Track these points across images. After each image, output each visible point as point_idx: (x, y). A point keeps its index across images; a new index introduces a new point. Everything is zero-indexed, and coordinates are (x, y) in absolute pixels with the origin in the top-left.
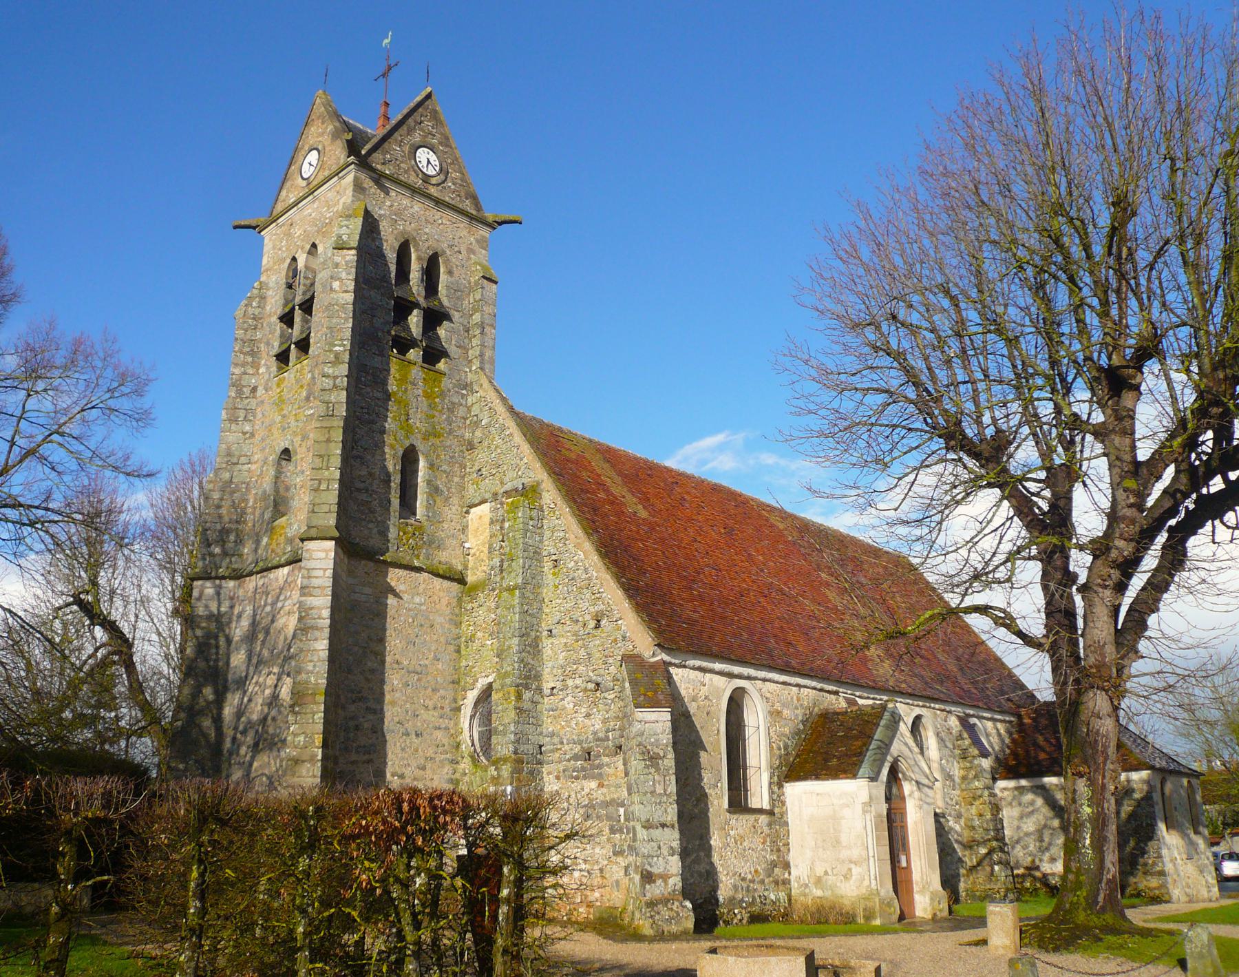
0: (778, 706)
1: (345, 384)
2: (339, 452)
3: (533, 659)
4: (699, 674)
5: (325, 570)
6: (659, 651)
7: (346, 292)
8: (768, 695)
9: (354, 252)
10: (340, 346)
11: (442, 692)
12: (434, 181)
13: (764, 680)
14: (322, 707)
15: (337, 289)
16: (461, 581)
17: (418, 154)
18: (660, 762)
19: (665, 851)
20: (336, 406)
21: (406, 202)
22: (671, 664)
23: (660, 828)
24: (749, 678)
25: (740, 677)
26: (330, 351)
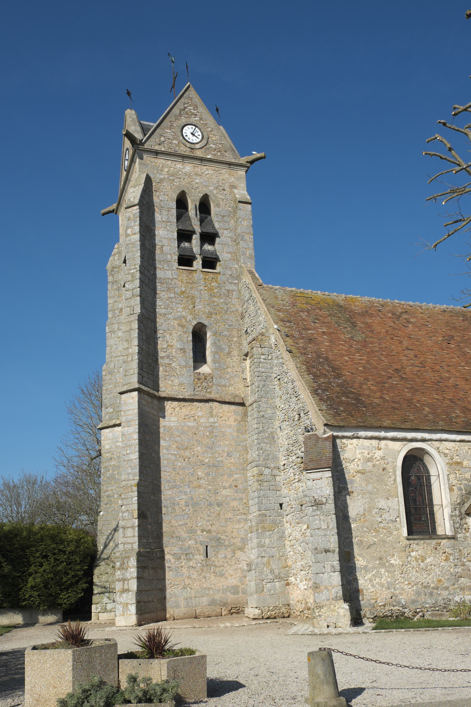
0: (456, 459)
1: (139, 292)
2: (137, 335)
3: (270, 447)
4: (375, 442)
5: (134, 409)
6: (327, 430)
7: (135, 234)
8: (447, 451)
9: (137, 207)
10: (133, 269)
11: (236, 476)
12: (198, 146)
13: (441, 440)
14: (136, 494)
15: (130, 233)
16: (242, 404)
17: (184, 131)
18: (323, 506)
19: (328, 568)
20: (134, 307)
21: (179, 166)
22: (337, 437)
23: (324, 553)
24: (423, 440)
25: (412, 440)
26: (129, 274)
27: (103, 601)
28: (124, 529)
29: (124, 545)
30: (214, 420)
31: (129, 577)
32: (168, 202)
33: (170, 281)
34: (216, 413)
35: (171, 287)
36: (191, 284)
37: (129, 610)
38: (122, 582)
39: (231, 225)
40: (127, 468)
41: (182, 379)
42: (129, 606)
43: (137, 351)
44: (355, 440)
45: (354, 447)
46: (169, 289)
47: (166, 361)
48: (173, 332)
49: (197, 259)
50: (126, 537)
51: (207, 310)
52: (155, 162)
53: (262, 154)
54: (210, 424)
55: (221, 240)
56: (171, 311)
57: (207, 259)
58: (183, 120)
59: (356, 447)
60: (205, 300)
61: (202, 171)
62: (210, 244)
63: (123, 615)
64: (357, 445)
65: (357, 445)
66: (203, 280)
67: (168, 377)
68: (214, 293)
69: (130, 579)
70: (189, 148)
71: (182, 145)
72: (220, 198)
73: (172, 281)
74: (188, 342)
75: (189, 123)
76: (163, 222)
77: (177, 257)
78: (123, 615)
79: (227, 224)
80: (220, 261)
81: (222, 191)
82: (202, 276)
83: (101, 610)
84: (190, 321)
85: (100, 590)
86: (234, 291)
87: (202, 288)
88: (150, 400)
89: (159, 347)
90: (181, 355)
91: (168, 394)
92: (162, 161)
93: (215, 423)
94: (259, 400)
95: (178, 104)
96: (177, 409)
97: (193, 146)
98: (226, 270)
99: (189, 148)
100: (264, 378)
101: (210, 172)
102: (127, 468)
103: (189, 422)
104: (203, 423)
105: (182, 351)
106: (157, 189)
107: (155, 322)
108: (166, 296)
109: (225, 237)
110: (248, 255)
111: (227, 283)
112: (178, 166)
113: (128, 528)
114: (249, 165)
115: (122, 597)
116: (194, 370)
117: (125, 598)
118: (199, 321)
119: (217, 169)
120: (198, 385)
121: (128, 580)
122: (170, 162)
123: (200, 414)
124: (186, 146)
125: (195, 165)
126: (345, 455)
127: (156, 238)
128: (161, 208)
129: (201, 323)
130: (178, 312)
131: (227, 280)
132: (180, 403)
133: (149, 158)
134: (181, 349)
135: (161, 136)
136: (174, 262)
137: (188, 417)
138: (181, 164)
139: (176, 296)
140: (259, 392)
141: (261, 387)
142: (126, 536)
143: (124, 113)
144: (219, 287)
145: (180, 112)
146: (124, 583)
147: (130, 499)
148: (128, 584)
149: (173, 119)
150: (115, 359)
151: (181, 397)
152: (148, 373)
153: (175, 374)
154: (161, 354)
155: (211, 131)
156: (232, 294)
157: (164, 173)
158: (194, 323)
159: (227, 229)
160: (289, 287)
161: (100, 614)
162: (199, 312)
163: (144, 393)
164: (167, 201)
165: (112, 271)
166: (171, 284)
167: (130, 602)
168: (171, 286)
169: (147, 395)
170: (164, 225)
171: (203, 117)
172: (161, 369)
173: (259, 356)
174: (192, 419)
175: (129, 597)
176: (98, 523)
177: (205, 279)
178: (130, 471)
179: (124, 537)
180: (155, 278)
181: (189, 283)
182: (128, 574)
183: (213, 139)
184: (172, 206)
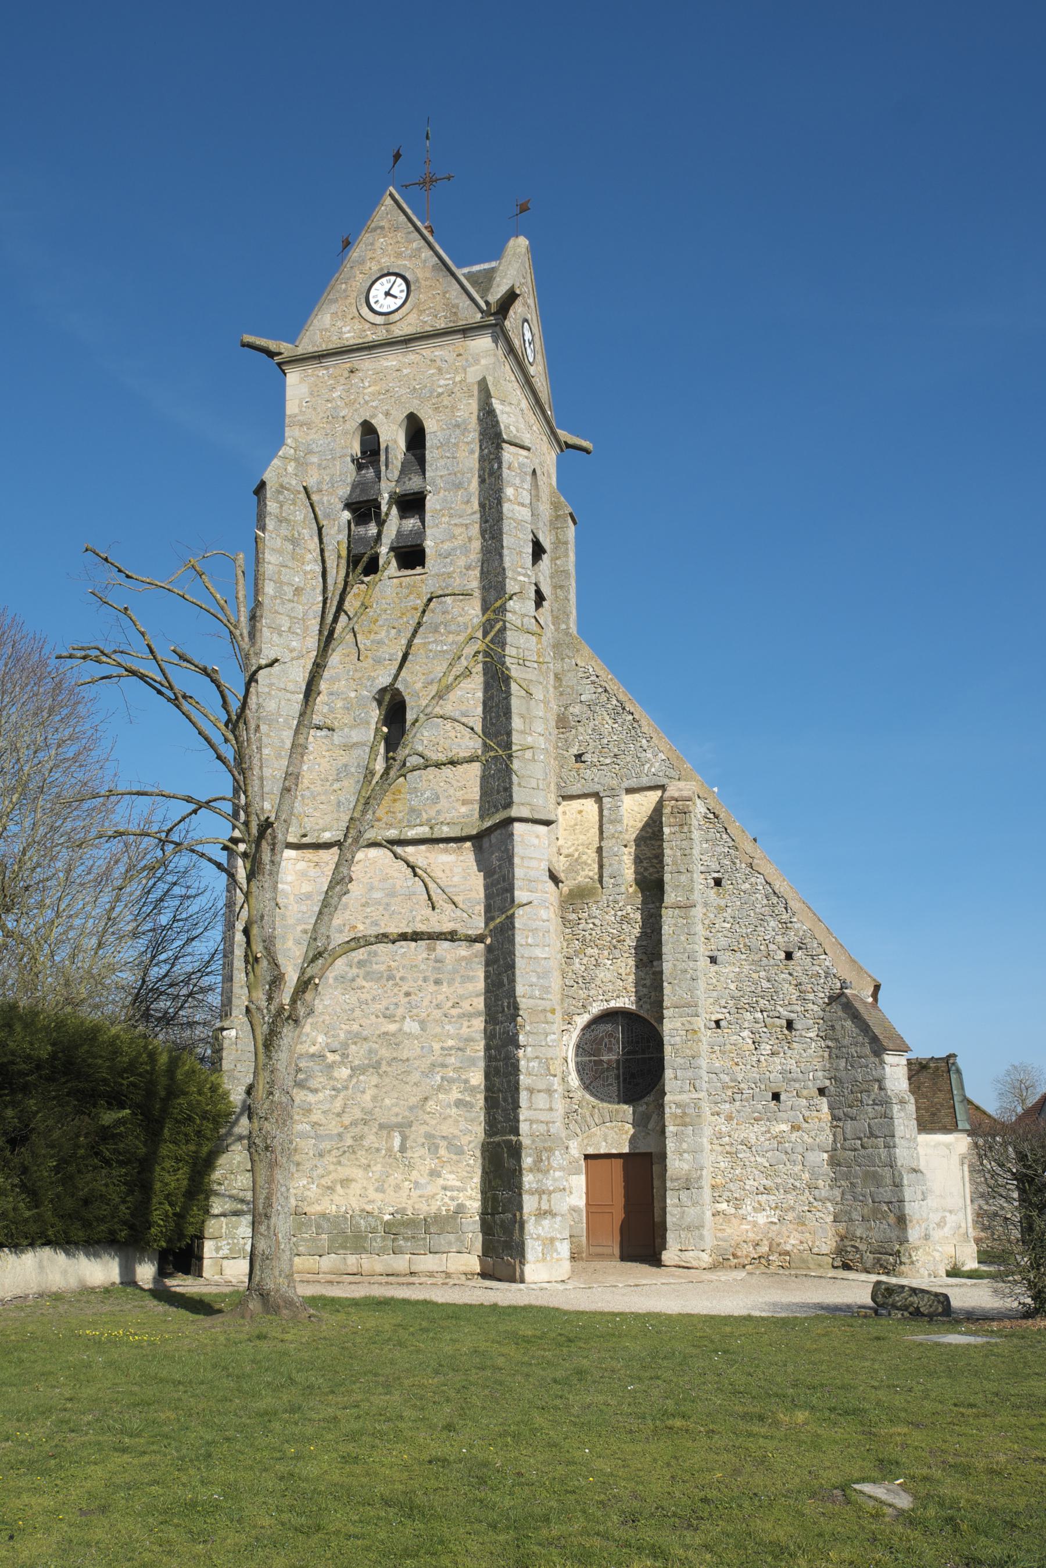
5: (541, 860)
27: (238, 1232)
28: (532, 1093)
29: (531, 1124)
31: (551, 1188)
37: (556, 1251)
38: (537, 1196)
40: (527, 973)
42: (557, 1244)
50: (535, 1110)
63: (544, 1259)
69: (554, 1191)
78: (544, 1259)
83: (231, 1253)
85: (229, 1206)
102: (527, 973)
113: (539, 1091)
115: (541, 1225)
117: (546, 1228)
121: (550, 1193)
142: (534, 1106)
143: (507, 240)
146: (540, 1198)
147: (543, 1037)
148: (549, 1201)
150: (280, 694)
161: (225, 1262)
165: (279, 492)
167: (558, 1236)
175: (556, 1226)
176: (225, 1054)
178: (534, 980)
179: (530, 1108)
182: (549, 1182)
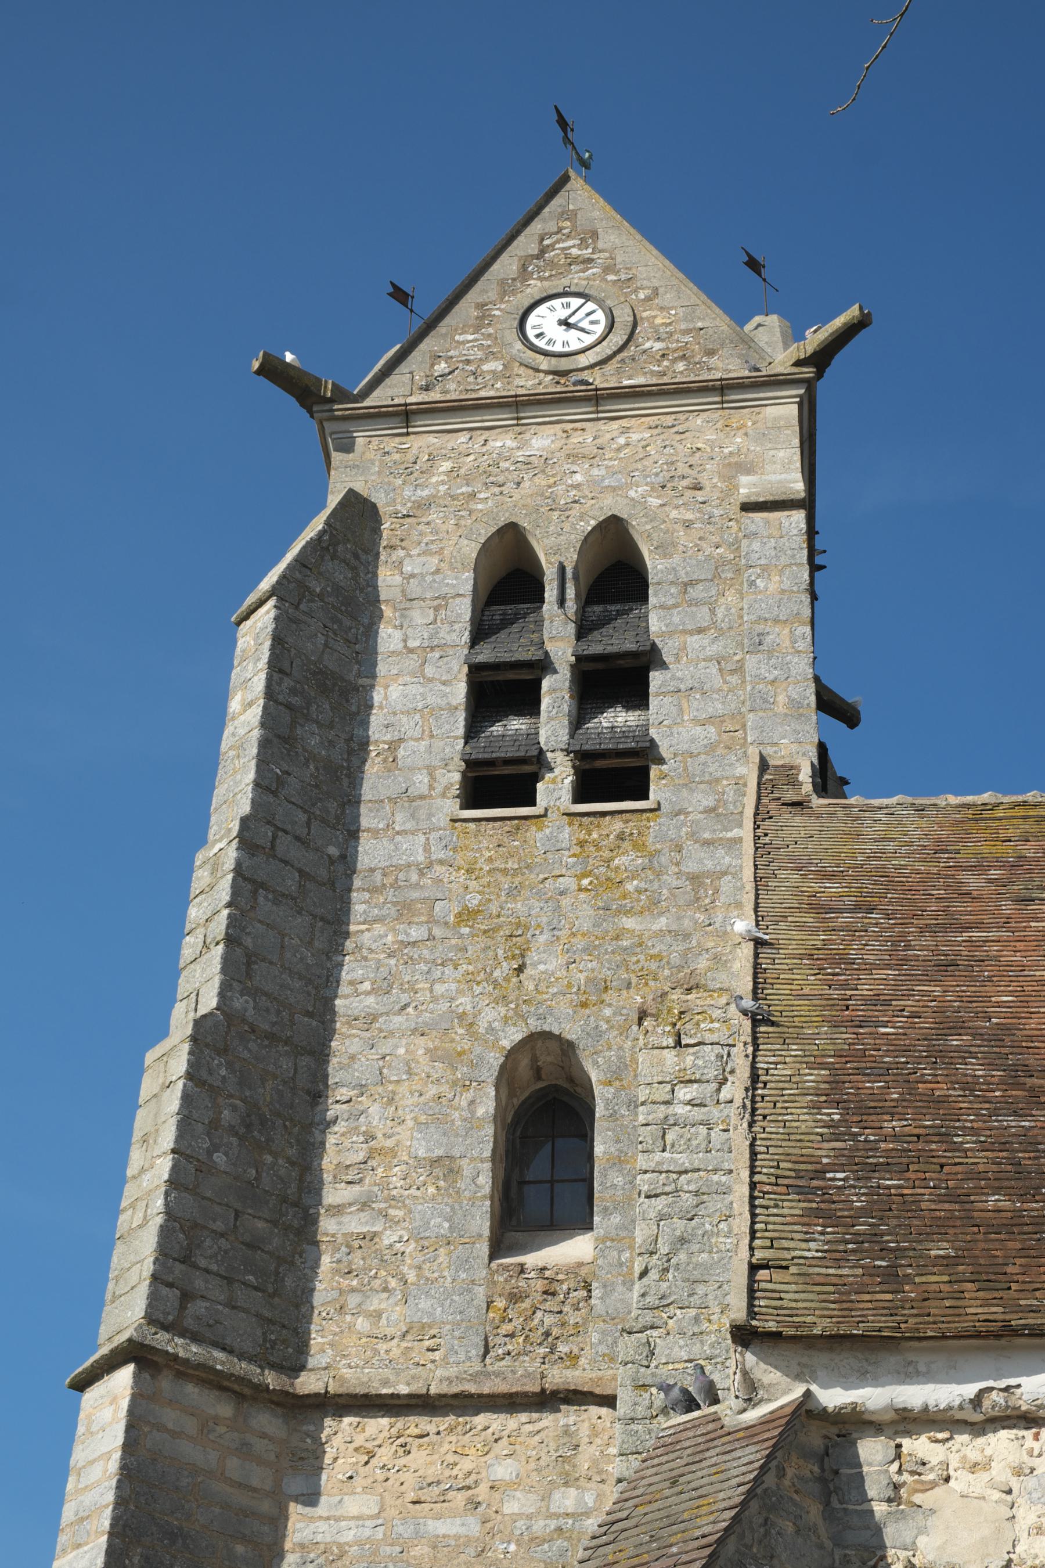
6: (768, 1375)
21: (502, 442)
30: (580, 1501)
32: (438, 578)
33: (414, 877)
34: (595, 1462)
35: (417, 900)
36: (516, 872)
39: (720, 612)
41: (424, 1304)
43: (166, 1177)
44: (1004, 1434)
45: (992, 1485)
46: (405, 911)
47: (355, 1224)
48: (403, 1089)
49: (551, 770)
51: (582, 977)
52: (399, 451)
53: (853, 312)
54: (553, 1524)
55: (673, 678)
56: (405, 998)
57: (600, 764)
58: (535, 288)
59: (1014, 1483)
60: (574, 935)
61: (598, 441)
62: (629, 707)
64: (1018, 1472)
65: (1018, 1472)
66: (577, 850)
67: (353, 1301)
68: (625, 897)
70: (548, 373)
71: (522, 371)
72: (676, 521)
73: (422, 874)
74: (471, 1123)
75: (551, 292)
76: (411, 651)
77: (457, 777)
79: (705, 609)
80: (661, 761)
81: (689, 493)
82: (567, 834)
84: (490, 1029)
86: (725, 873)
87: (568, 882)
88: (225, 1409)
89: (328, 1162)
90: (432, 1190)
91: (343, 1380)
92: (432, 439)
93: (587, 1514)
94: (648, 1318)
95: (515, 243)
96: (385, 1455)
97: (564, 364)
98: (692, 791)
99: (548, 373)
100: (688, 1200)
101: (635, 437)
103: (438, 1517)
104: (515, 1518)
105: (438, 1171)
106: (395, 541)
107: (320, 1053)
108: (390, 938)
109: (690, 661)
110: (780, 709)
111: (689, 846)
112: (499, 444)
114: (808, 372)
116: (492, 1257)
118: (534, 1025)
119: (669, 420)
120: (507, 1328)
122: (463, 438)
123: (503, 1471)
124: (537, 370)
125: (569, 426)
126: (922, 1541)
127: (373, 718)
128: (408, 604)
129: (546, 1036)
130: (435, 999)
131: (692, 835)
132: (400, 1423)
133: (375, 441)
134: (436, 1161)
135: (437, 358)
136: (443, 795)
137: (436, 1490)
138: (511, 435)
139: (437, 932)
140: (653, 1275)
141: (664, 1249)
144: (653, 868)
145: (524, 268)
149: (493, 295)
151: (403, 1389)
152: (230, 1281)
153: (393, 1283)
154: (333, 1195)
155: (648, 299)
156: (717, 891)
157: (434, 480)
158: (513, 1036)
159: (700, 631)
160: (956, 795)
162: (542, 987)
163: (180, 1375)
164: (437, 571)
166: (416, 886)
168: (415, 894)
169: (202, 1382)
170: (412, 662)
171: (619, 259)
172: (326, 1260)
173: (662, 1093)
174: (459, 1499)
177: (582, 844)
180: (351, 871)
181: (505, 872)
183: (658, 321)
184: (454, 586)
